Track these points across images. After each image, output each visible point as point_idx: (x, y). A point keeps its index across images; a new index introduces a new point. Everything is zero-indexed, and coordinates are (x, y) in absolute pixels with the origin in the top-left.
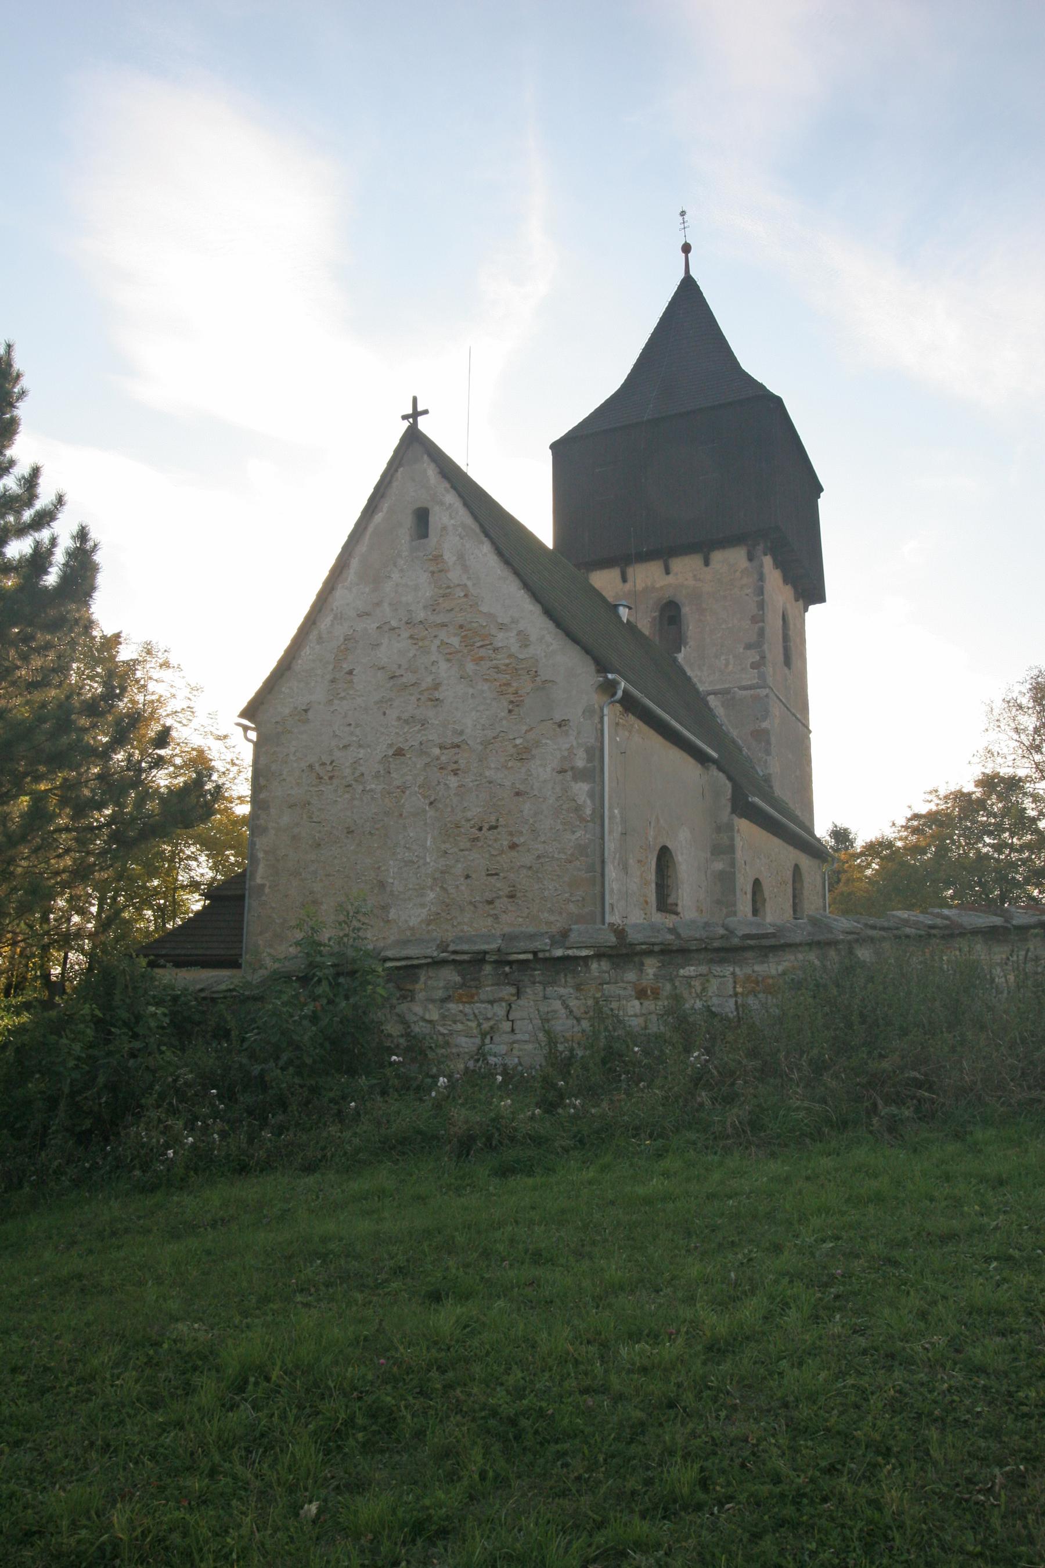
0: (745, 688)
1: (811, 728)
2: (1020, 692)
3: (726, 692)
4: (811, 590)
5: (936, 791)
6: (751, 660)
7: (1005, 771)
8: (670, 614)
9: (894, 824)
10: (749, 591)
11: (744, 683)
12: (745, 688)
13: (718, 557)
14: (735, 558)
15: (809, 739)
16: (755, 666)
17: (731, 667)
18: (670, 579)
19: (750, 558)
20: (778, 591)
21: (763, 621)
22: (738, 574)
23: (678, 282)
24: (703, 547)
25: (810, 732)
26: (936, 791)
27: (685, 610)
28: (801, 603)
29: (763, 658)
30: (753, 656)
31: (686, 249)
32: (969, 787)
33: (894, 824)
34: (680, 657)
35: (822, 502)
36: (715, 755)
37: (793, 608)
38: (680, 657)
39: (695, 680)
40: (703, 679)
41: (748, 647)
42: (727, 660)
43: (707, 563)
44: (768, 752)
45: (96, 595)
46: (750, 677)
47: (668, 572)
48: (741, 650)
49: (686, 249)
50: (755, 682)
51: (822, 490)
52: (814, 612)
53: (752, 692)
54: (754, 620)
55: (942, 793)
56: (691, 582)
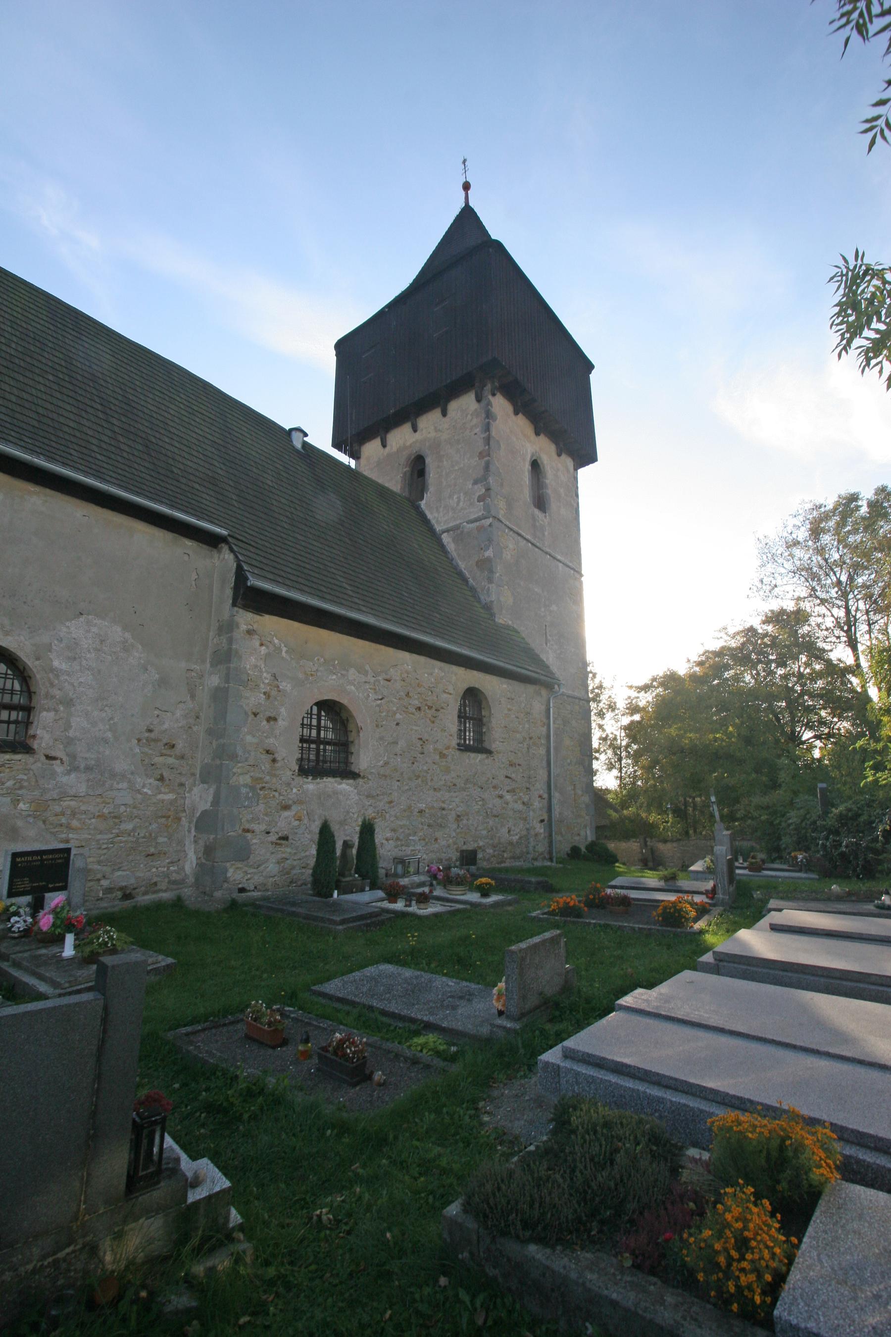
0: (472, 522)
1: (583, 572)
2: (794, 526)
3: (457, 527)
4: (585, 454)
5: (725, 629)
6: (477, 494)
7: (790, 606)
8: (418, 468)
9: (689, 661)
10: (477, 430)
11: (472, 517)
12: (472, 522)
13: (454, 406)
14: (465, 405)
15: (581, 583)
16: (481, 499)
17: (461, 504)
18: (418, 436)
19: (479, 400)
20: (518, 437)
21: (489, 455)
22: (469, 417)
23: (457, 212)
24: (438, 400)
25: (581, 575)
26: (725, 629)
27: (428, 460)
28: (570, 463)
29: (488, 489)
30: (480, 490)
31: (466, 187)
32: (756, 622)
33: (689, 661)
34: (423, 504)
35: (593, 376)
36: (224, 532)
37: (555, 464)
38: (423, 504)
39: (433, 522)
40: (439, 519)
41: (476, 482)
42: (459, 498)
43: (444, 414)
44: (490, 580)
45: (682, 661)
46: (477, 510)
47: (415, 430)
48: (470, 486)
49: (466, 187)
50: (480, 514)
51: (590, 367)
52: (585, 474)
53: (478, 524)
54: (481, 455)
55: (732, 631)
56: (433, 434)
